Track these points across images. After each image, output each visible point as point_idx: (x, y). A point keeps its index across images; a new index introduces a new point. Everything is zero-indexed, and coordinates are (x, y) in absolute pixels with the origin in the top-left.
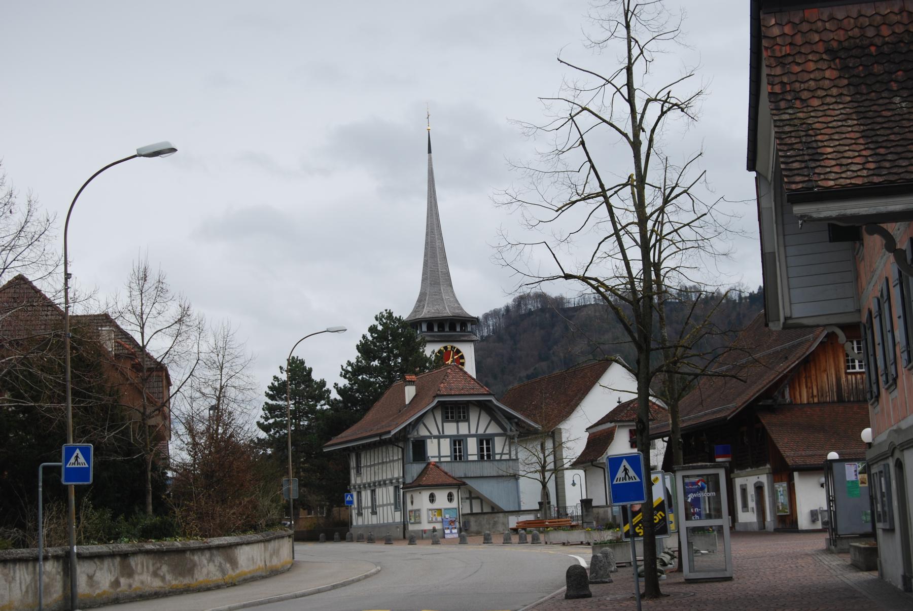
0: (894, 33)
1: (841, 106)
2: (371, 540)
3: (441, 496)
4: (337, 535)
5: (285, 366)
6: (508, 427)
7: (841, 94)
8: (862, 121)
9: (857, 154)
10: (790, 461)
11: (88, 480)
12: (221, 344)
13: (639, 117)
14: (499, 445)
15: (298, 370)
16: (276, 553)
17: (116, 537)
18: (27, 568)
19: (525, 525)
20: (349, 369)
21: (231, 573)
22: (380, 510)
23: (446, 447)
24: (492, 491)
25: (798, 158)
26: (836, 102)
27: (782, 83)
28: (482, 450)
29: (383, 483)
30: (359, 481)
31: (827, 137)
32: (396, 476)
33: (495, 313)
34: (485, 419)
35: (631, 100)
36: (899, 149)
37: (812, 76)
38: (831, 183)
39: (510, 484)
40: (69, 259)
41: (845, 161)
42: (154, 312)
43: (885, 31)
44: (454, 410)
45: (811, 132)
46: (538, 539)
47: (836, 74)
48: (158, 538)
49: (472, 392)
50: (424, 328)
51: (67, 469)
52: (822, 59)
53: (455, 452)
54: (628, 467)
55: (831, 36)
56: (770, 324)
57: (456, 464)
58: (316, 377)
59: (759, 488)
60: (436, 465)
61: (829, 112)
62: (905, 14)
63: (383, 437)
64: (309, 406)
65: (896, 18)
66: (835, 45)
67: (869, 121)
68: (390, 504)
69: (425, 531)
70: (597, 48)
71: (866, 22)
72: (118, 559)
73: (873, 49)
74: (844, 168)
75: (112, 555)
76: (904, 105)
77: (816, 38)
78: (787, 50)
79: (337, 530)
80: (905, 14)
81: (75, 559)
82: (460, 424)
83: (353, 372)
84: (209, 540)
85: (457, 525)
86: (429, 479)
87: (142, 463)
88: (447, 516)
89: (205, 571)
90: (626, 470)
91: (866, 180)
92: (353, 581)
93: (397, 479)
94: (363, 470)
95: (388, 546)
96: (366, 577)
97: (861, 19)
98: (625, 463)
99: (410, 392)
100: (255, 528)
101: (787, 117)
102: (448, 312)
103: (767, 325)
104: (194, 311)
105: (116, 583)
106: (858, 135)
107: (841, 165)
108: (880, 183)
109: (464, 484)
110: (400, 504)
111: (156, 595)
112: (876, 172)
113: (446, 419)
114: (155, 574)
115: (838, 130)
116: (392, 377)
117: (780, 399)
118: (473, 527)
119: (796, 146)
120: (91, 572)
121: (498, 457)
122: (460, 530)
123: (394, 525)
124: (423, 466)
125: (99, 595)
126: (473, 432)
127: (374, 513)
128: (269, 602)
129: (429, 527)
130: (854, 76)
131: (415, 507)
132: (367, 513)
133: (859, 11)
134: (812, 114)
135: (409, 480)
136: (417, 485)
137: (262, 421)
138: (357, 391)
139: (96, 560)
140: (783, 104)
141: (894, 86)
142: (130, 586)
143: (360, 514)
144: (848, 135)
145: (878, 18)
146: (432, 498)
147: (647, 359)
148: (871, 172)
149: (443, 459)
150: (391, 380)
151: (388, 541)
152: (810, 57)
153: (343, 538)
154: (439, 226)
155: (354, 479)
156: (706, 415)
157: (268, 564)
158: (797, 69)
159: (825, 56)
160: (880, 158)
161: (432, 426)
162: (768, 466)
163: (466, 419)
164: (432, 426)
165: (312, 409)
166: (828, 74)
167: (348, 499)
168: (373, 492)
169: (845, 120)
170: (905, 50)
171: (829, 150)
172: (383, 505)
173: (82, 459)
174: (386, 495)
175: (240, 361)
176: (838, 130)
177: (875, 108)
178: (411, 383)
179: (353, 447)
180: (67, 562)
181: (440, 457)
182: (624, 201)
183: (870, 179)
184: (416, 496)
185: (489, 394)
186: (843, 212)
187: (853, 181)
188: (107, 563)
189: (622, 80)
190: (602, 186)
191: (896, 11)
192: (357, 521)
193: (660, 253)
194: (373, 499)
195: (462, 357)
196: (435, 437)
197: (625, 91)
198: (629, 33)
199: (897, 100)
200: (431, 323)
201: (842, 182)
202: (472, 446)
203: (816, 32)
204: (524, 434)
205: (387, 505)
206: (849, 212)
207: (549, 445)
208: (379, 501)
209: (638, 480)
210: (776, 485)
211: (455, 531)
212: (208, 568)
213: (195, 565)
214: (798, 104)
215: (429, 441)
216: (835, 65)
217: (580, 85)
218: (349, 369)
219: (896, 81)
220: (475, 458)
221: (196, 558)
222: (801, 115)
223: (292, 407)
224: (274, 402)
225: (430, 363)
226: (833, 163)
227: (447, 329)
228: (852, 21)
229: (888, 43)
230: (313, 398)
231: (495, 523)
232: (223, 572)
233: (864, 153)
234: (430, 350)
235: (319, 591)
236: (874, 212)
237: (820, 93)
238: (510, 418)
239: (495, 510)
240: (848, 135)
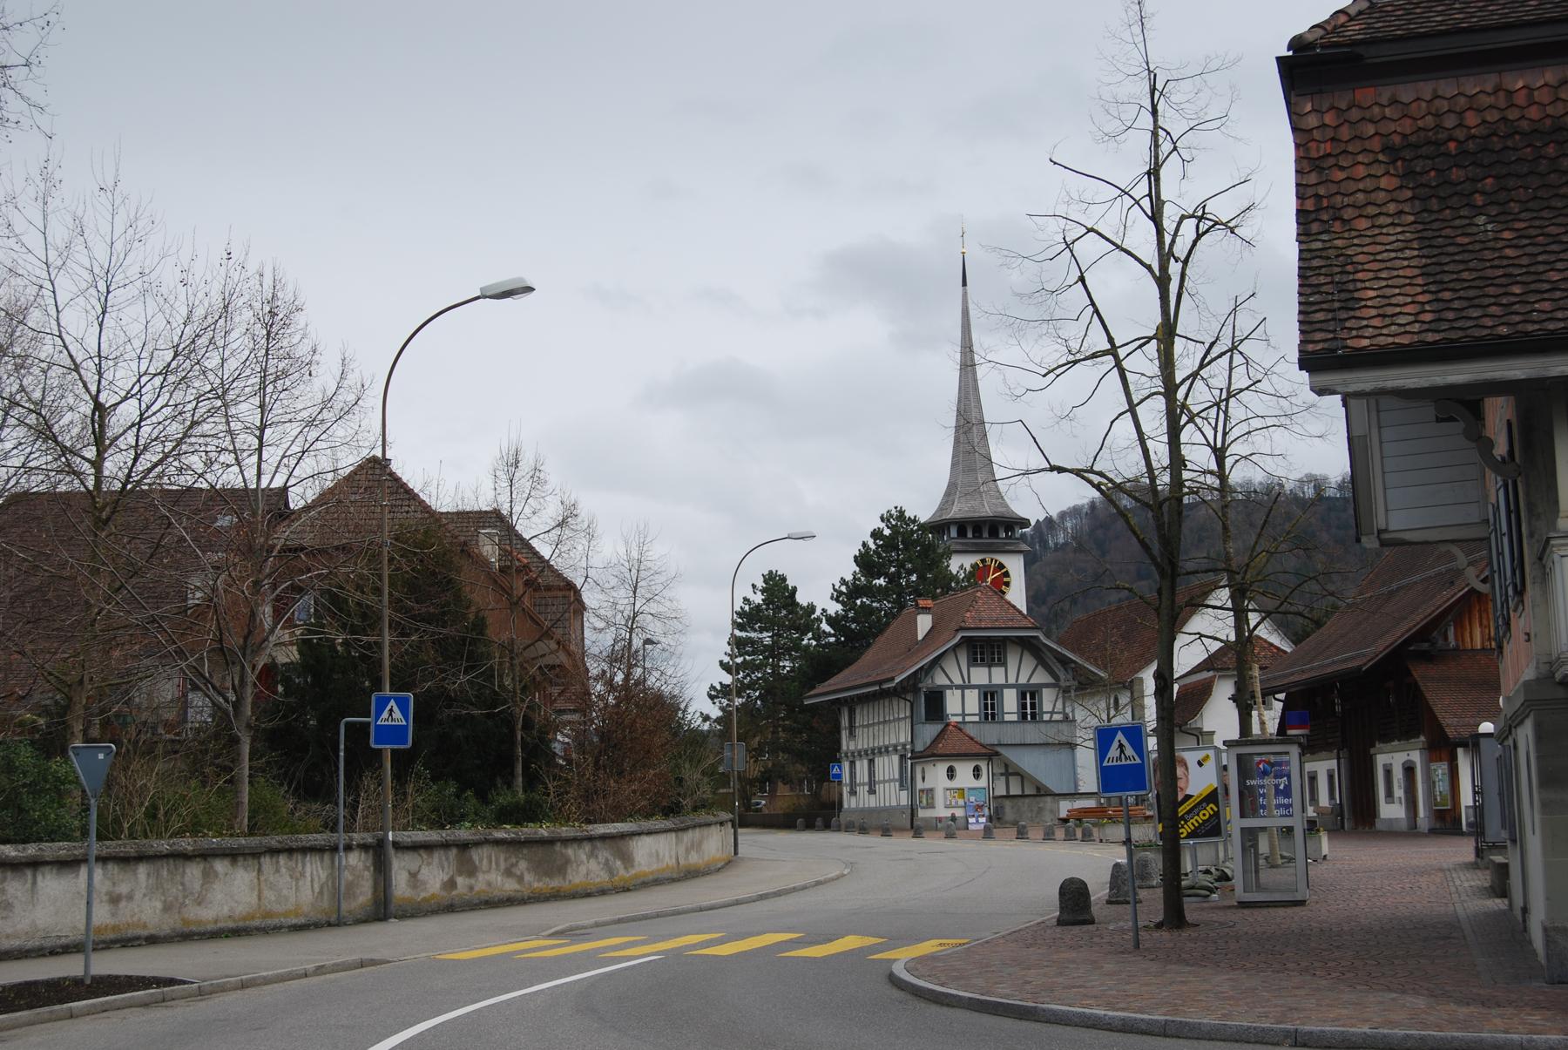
0: (1484, 122)
1: (1399, 229)
2: (863, 830)
3: (964, 770)
4: (819, 822)
5: (760, 584)
6: (1062, 677)
7: (1401, 212)
8: (1425, 252)
9: (1409, 299)
10: (1450, 732)
11: (405, 743)
12: (635, 554)
13: (1168, 239)
14: (1048, 700)
15: (777, 589)
16: (696, 846)
17: (455, 820)
18: (322, 861)
19: (1080, 816)
20: (843, 589)
21: (623, 873)
22: (879, 788)
23: (973, 701)
24: (1035, 764)
25: (1324, 306)
26: (1392, 224)
27: (1317, 196)
28: (1024, 706)
29: (884, 751)
30: (852, 747)
31: (1371, 275)
32: (902, 740)
33: (1075, 512)
34: (1029, 663)
35: (1156, 217)
36: (1471, 293)
37: (1361, 186)
38: (1366, 342)
39: (1064, 754)
40: (388, 439)
41: (1390, 310)
42: (527, 510)
43: (1471, 119)
44: (985, 650)
45: (1349, 268)
46: (1091, 834)
47: (1396, 182)
48: (518, 823)
49: (1010, 624)
50: (954, 533)
51: (377, 727)
52: (1377, 161)
54: (1124, 742)
55: (1392, 127)
56: (1364, 539)
57: (987, 726)
58: (802, 599)
59: (1409, 770)
60: (957, 726)
61: (1379, 239)
62: (1501, 94)
63: (885, 686)
64: (791, 640)
65: (1488, 100)
66: (1397, 139)
67: (1435, 251)
68: (894, 780)
69: (940, 820)
70: (1112, 144)
71: (1445, 105)
72: (454, 851)
73: (1452, 145)
74: (1388, 321)
75: (446, 846)
76: (1489, 227)
77: (1370, 130)
78: (1326, 148)
79: (820, 813)
80: (1501, 94)
81: (391, 851)
82: (994, 669)
83: (849, 593)
84: (590, 827)
85: (986, 811)
86: (948, 747)
87: (509, 721)
88: (972, 799)
89: (583, 869)
90: (1121, 746)
91: (1416, 338)
92: (795, 890)
93: (904, 746)
94: (858, 732)
95: (885, 839)
96: (818, 883)
97: (1437, 102)
98: (1120, 736)
99: (924, 623)
100: (671, 810)
101: (1319, 245)
102: (987, 510)
103: (1358, 540)
104: (584, 511)
105: (451, 884)
106: (1417, 272)
107: (1384, 316)
108: (1435, 342)
109: (997, 754)
110: (906, 781)
111: (510, 901)
112: (1433, 326)
113: (973, 662)
114: (508, 873)
115: (1388, 264)
116: (900, 598)
117: (1440, 642)
118: (1009, 814)
119: (1324, 289)
120: (414, 868)
121: (1046, 717)
122: (990, 819)
123: (898, 809)
124: (939, 727)
125: (425, 899)
126: (1012, 680)
127: (872, 791)
128: (658, 915)
129: (947, 813)
130: (1421, 185)
131: (927, 785)
132: (862, 791)
133: (1435, 90)
134: (1356, 241)
135: (919, 747)
136: (930, 754)
137: (726, 659)
138: (854, 620)
139: (422, 852)
140: (1315, 227)
141: (1479, 200)
142: (471, 888)
143: (853, 793)
144: (1401, 273)
145: (1462, 100)
146: (951, 773)
147: (1173, 588)
148: (1426, 327)
149: (968, 719)
150: (902, 607)
151: (886, 832)
152: (1360, 158)
153: (827, 826)
154: (976, 389)
155: (846, 744)
156: (1334, 663)
157: (682, 862)
158: (1341, 175)
159: (1381, 157)
160: (1441, 306)
161: (952, 672)
162: (1422, 738)
163: (1003, 663)
164: (952, 672)
165: (796, 645)
166: (1384, 183)
167: (835, 771)
168: (871, 762)
169: (1401, 250)
170: (1498, 147)
171: (1371, 294)
172: (884, 781)
173: (397, 714)
174: (888, 767)
175: (660, 579)
176: (1388, 264)
177: (1448, 232)
178: (926, 610)
179: (845, 699)
180: (379, 854)
181: (964, 715)
182: (1144, 364)
183: (1423, 337)
184: (930, 769)
185: (1035, 628)
186: (1381, 384)
187: (1397, 340)
188: (438, 855)
189: (1142, 189)
190: (1111, 340)
191: (1489, 90)
192: (849, 803)
193: (1225, 434)
194: (871, 773)
195: (1007, 574)
196: (958, 687)
197: (1146, 203)
198: (1155, 121)
199: (1481, 220)
200: (962, 526)
201: (1382, 340)
202: (1010, 700)
203: (1371, 121)
204: (1084, 686)
205: (890, 781)
206: (1390, 384)
207: (1124, 699)
208: (879, 776)
209: (1138, 761)
210: (1434, 766)
211: (982, 820)
212: (587, 867)
213: (568, 861)
214: (1337, 226)
215: (948, 692)
216: (1396, 169)
217: (1088, 197)
218: (843, 589)
219: (1483, 193)
220: (1014, 718)
221: (570, 852)
222: (1339, 243)
223: (767, 641)
224: (744, 634)
225: (957, 583)
226: (1373, 312)
227: (986, 534)
228: (1424, 105)
229: (1474, 137)
230: (797, 629)
231: (1040, 810)
232: (611, 871)
233: (1420, 298)
234: (959, 564)
235: (737, 903)
236: (1426, 385)
237: (1371, 210)
238: (1064, 662)
239: (1042, 792)
240: (1401, 273)
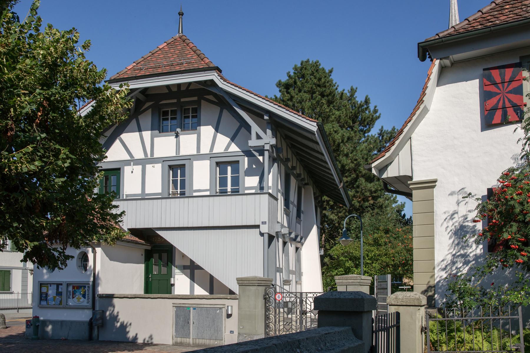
23: (155, 179)
53: (183, 182)
82: (183, 138)
196: (137, 162)
